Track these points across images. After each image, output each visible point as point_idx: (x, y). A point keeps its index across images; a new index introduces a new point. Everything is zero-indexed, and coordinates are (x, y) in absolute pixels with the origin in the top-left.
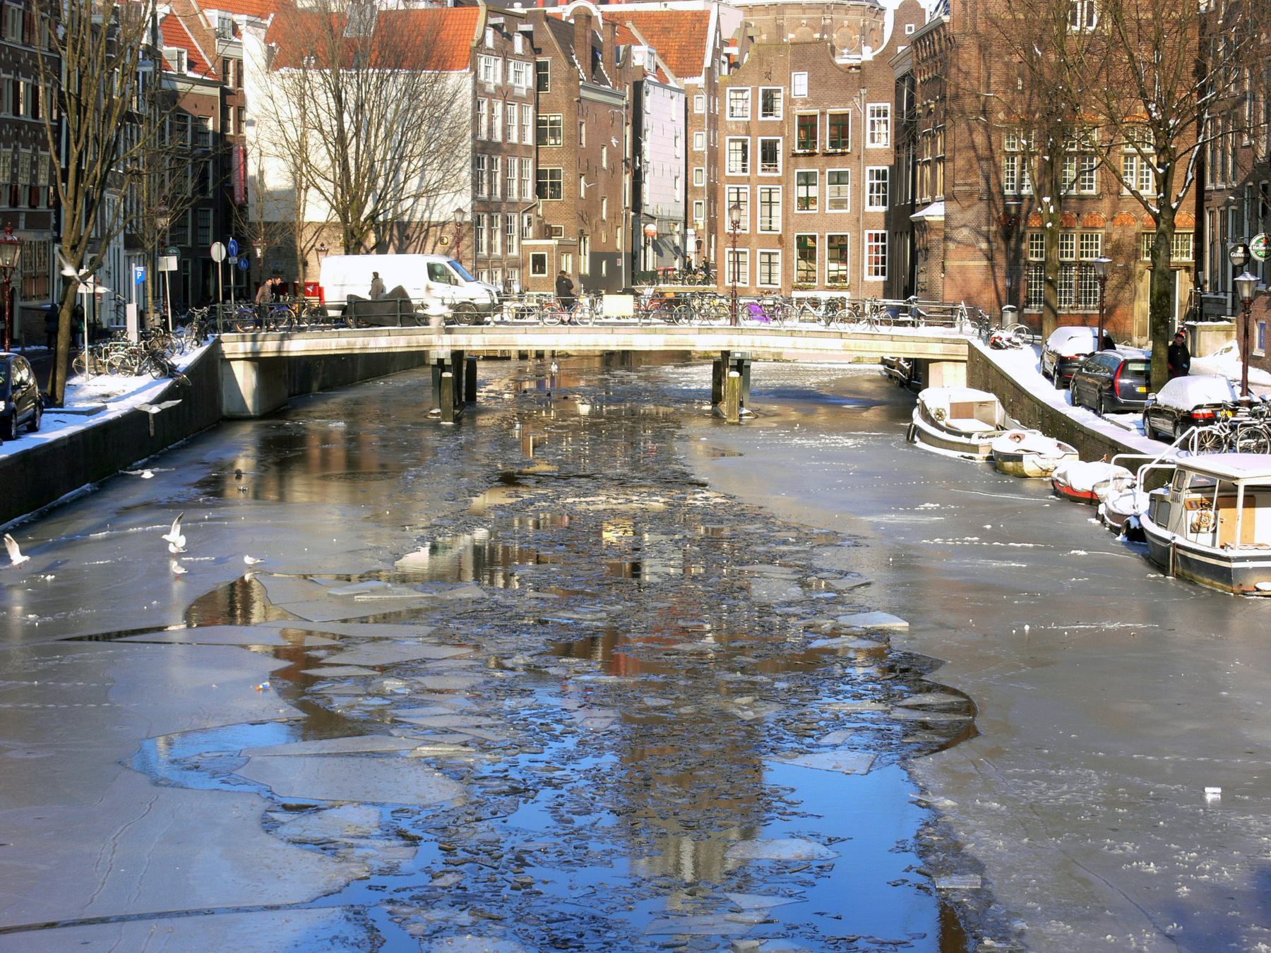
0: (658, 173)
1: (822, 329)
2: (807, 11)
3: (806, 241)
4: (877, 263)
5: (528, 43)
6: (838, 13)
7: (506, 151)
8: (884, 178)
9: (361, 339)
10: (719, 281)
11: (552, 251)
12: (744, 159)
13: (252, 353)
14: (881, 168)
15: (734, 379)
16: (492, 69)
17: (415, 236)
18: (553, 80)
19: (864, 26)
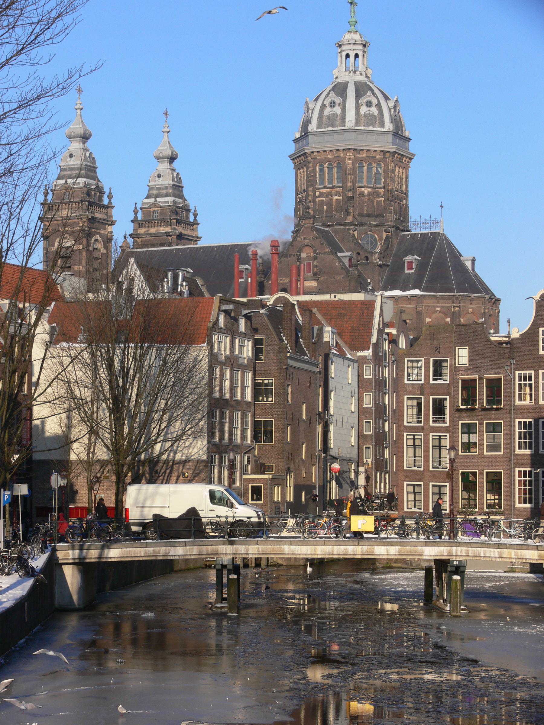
0: (339, 424)
1: (522, 543)
2: (440, 301)
3: (468, 476)
4: (525, 494)
5: (249, 325)
6: (465, 303)
7: (232, 406)
8: (530, 428)
9: (164, 548)
10: (399, 507)
11: (267, 484)
12: (419, 412)
13: (79, 558)
14: (528, 420)
15: (456, 581)
16: (223, 344)
17: (163, 471)
19: (484, 312)
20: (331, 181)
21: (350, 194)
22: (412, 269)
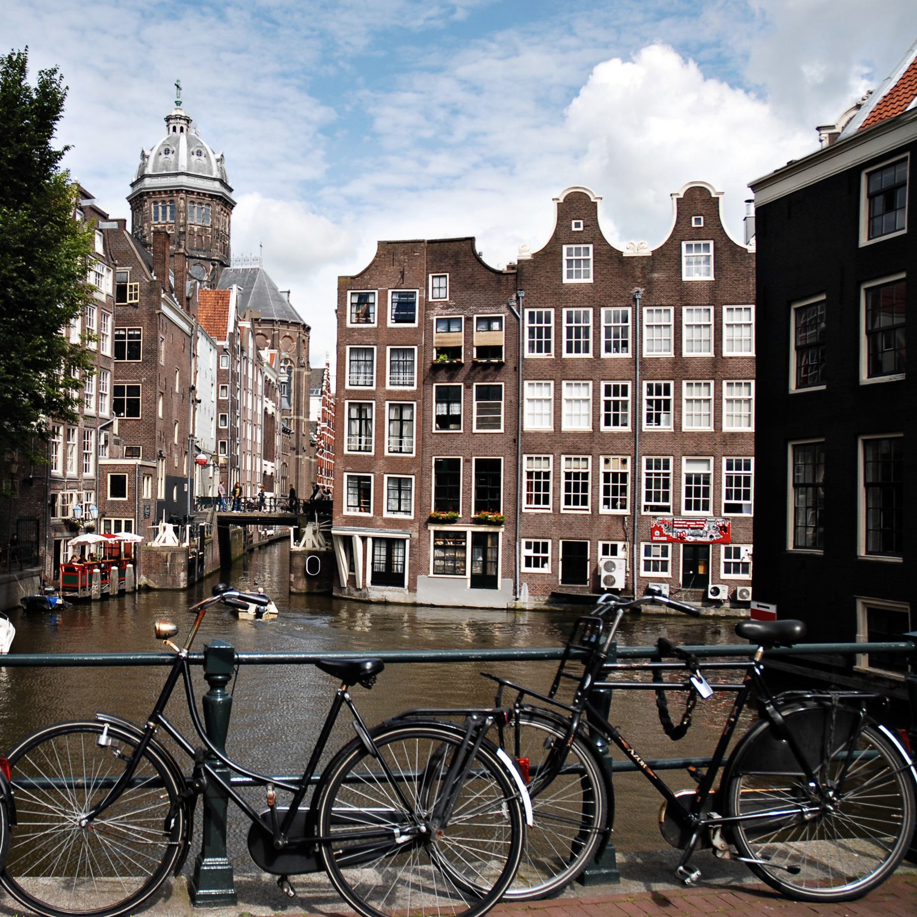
20: (164, 218)
21: (182, 230)
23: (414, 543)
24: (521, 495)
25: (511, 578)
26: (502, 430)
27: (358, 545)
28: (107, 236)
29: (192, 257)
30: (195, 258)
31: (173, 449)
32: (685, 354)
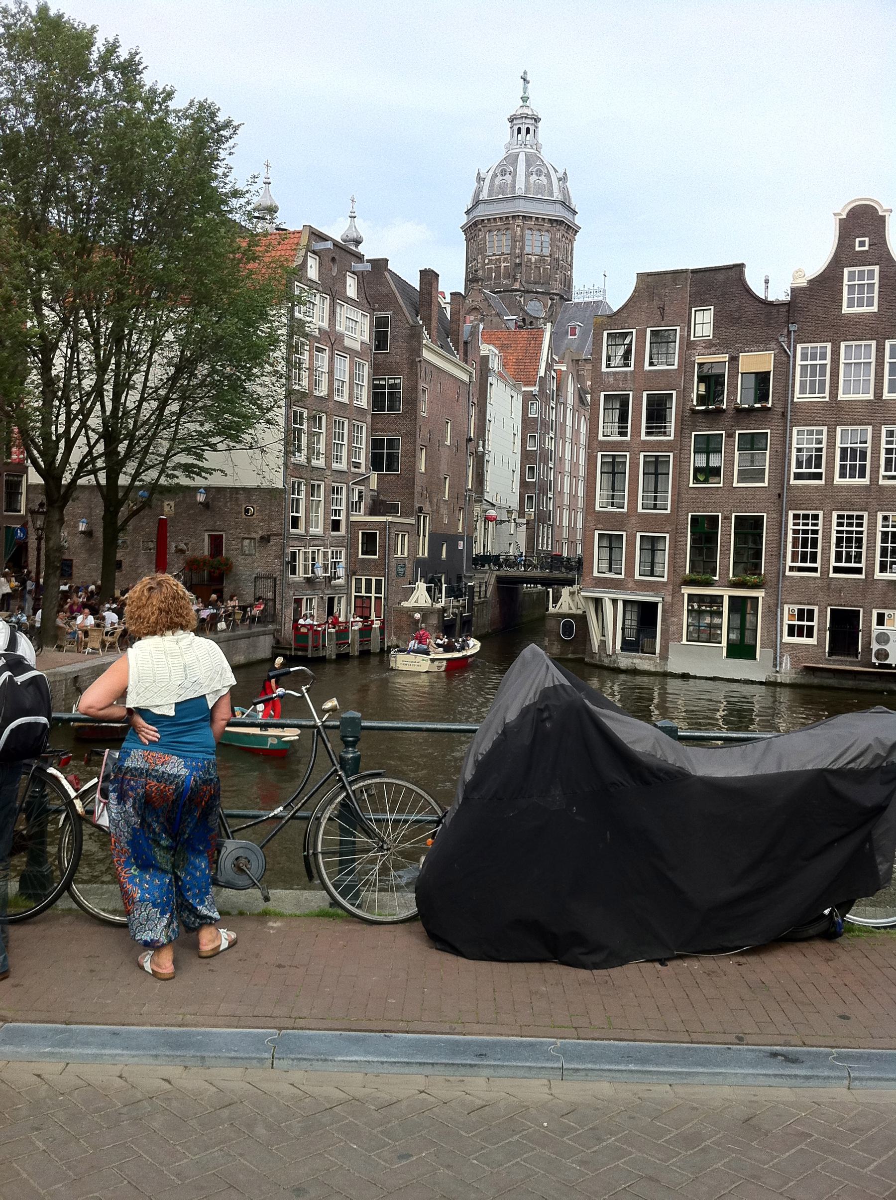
12: (623, 418)
18: (393, 337)
21: (518, 261)
22: (575, 335)
23: (666, 607)
24: (785, 552)
25: (771, 648)
26: (766, 484)
27: (608, 606)
28: (361, 278)
29: (528, 292)
30: (533, 292)
31: (442, 505)
32: (841, 397)
